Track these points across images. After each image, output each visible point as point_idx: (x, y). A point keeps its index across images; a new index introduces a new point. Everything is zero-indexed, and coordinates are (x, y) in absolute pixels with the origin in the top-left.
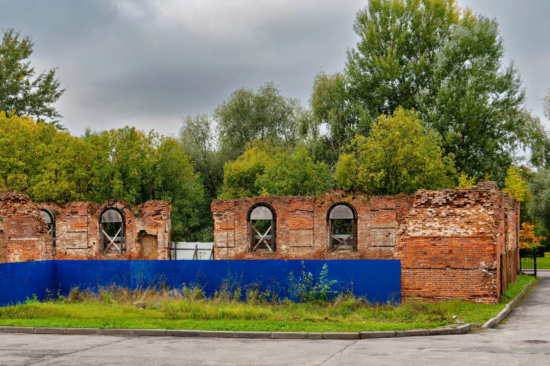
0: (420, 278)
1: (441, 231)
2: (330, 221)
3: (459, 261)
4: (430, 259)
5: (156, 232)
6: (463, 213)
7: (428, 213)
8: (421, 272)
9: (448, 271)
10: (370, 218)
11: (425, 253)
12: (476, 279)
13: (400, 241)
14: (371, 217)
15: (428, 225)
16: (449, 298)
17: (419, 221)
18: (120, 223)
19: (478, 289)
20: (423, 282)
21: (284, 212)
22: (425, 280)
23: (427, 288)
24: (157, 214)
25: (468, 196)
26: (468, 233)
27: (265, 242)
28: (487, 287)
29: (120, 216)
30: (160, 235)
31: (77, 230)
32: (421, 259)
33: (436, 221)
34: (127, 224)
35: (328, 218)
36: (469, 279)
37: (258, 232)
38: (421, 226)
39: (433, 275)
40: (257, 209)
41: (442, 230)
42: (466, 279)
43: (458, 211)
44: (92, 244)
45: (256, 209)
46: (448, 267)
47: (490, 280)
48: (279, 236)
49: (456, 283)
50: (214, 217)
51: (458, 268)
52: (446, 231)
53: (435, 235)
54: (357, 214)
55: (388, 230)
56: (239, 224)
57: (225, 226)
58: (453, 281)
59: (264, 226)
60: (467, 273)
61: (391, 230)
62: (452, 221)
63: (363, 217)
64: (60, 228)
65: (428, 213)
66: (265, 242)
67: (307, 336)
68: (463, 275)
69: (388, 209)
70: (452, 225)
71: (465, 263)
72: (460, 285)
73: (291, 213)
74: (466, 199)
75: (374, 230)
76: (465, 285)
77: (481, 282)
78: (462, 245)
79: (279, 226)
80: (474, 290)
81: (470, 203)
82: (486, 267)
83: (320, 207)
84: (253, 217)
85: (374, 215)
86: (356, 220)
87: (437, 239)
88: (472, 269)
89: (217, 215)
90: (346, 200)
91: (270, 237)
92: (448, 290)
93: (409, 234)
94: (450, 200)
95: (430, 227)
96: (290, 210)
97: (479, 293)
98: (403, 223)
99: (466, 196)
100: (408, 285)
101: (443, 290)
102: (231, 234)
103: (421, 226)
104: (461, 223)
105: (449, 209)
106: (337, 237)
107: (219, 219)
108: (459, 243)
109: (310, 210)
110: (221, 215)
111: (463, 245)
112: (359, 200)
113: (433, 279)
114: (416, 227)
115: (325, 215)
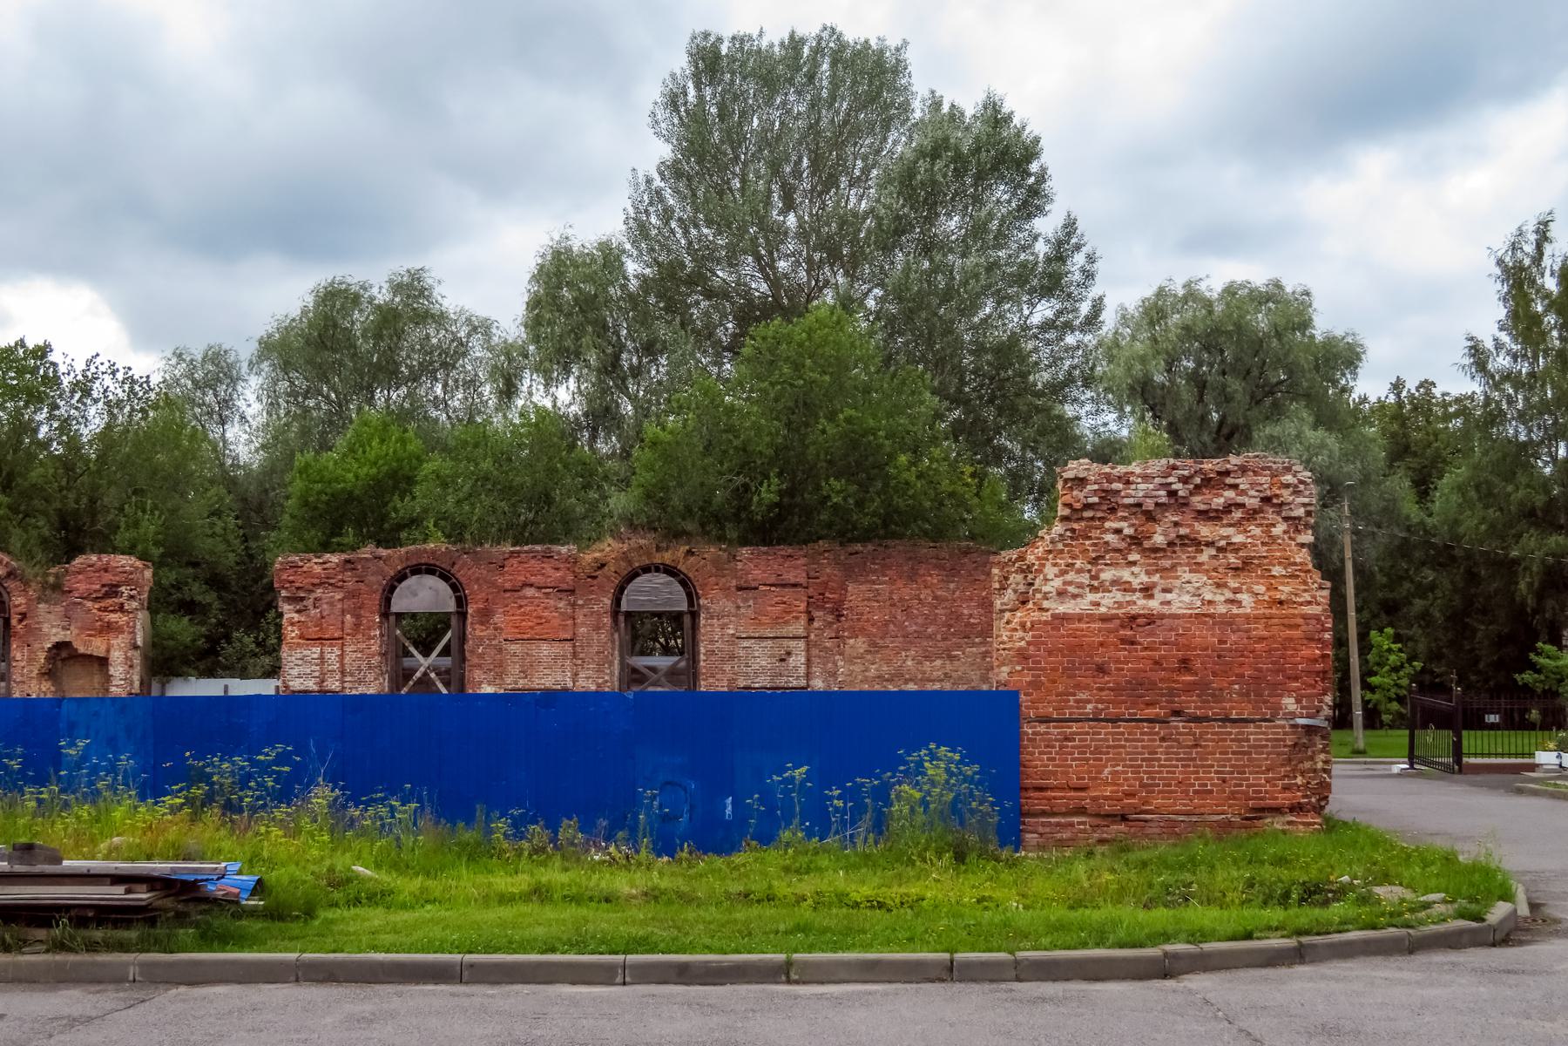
0: (1082, 749)
1: (1151, 597)
2: (621, 618)
4: (1117, 689)
6: (1223, 538)
7: (1109, 537)
8: (1088, 733)
9: (1177, 728)
10: (733, 610)
11: (1101, 669)
12: (1268, 754)
13: (1016, 630)
14: (738, 607)
15: (1107, 575)
16: (1181, 818)
17: (1078, 563)
19: (1275, 785)
20: (1094, 766)
21: (491, 590)
22: (1101, 760)
23: (1107, 784)
24: (107, 596)
25: (1238, 481)
26: (1239, 603)
27: (433, 675)
28: (1299, 780)
30: (117, 656)
32: (1087, 687)
33: (1134, 563)
34: (14, 622)
35: (615, 612)
37: (412, 649)
38: (1085, 579)
39: (1126, 740)
40: (412, 581)
41: (1156, 592)
42: (1233, 753)
43: (1205, 531)
45: (405, 584)
46: (1177, 713)
47: (1312, 758)
48: (472, 660)
49: (1203, 766)
50: (280, 604)
51: (1206, 719)
52: (1169, 596)
53: (1134, 610)
54: (698, 598)
55: (786, 642)
56: (357, 626)
57: (313, 631)
58: (1194, 759)
59: (427, 632)
60: (1238, 733)
61: (793, 643)
62: (1188, 564)
63: (715, 608)
65: (1109, 537)
66: (433, 675)
67: (951, 969)
68: (1225, 740)
69: (784, 586)
70: (1187, 576)
72: (1217, 772)
73: (508, 595)
74: (1230, 494)
75: (746, 644)
76: (1232, 773)
77: (1282, 765)
78: (1220, 642)
79: (475, 631)
80: (1260, 792)
81: (1242, 505)
83: (594, 578)
84: (400, 604)
85: (745, 600)
86: (694, 615)
88: (1253, 721)
89: (289, 600)
90: (666, 557)
91: (447, 662)
92: (1176, 792)
93: (1046, 604)
94: (1181, 493)
95: (1115, 582)
96: (508, 585)
97: (1277, 798)
98: (1016, 572)
99: (1229, 481)
100: (1046, 775)
101: (1160, 792)
102: (332, 654)
103: (1085, 579)
104: (1215, 570)
105: (1176, 524)
106: (641, 662)
107: (298, 612)
108: (1213, 635)
109: (564, 586)
110: (302, 599)
111: (1225, 642)
112: (702, 558)
113: (1128, 753)
114: (1070, 583)
115: (607, 601)
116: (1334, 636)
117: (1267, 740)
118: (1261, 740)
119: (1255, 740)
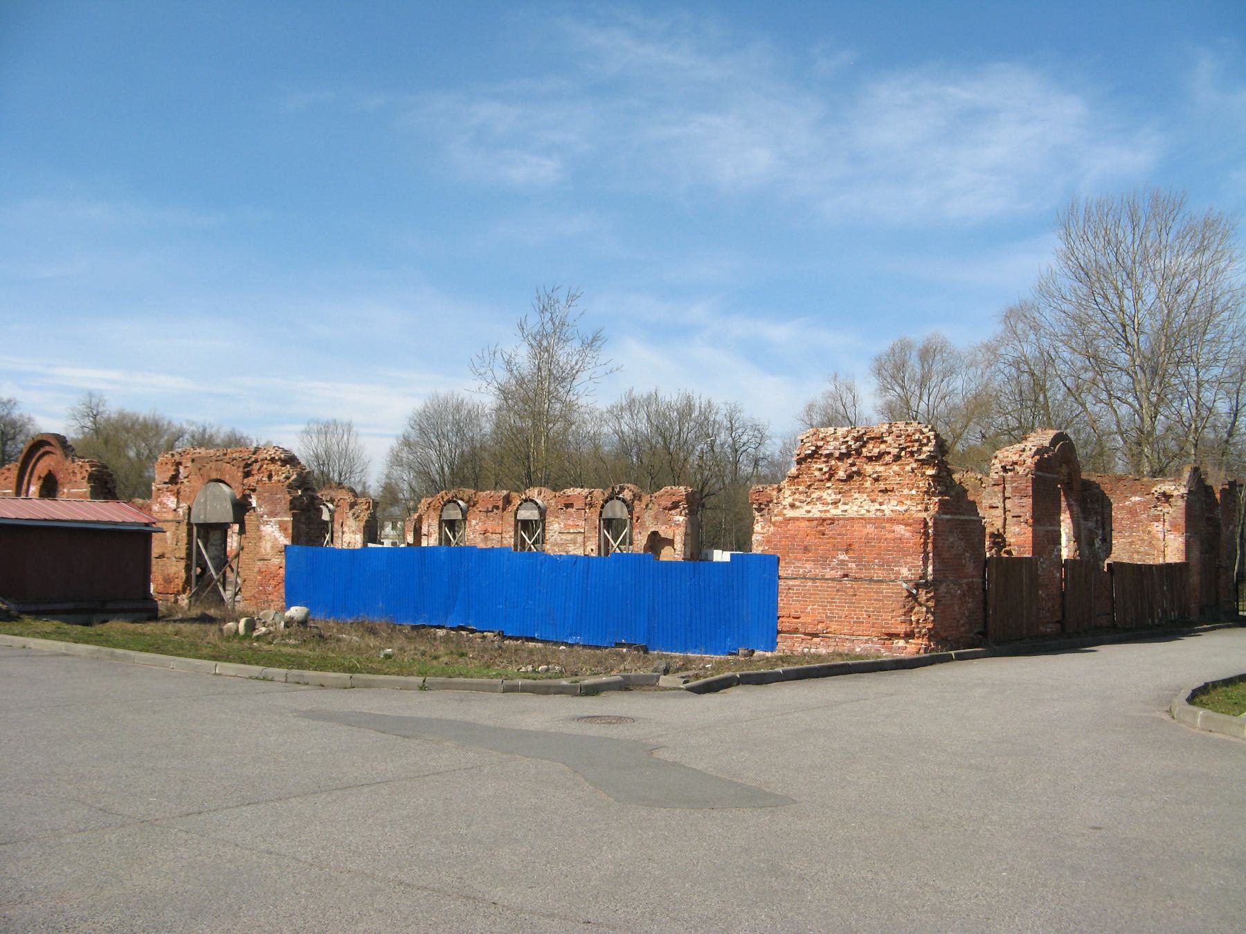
5: (672, 535)
7: (817, 473)
9: (846, 584)
18: (625, 520)
22: (807, 601)
29: (625, 510)
31: (571, 531)
36: (880, 600)
42: (875, 600)
44: (590, 551)
49: (858, 607)
64: (551, 528)
68: (870, 592)
70: (856, 495)
71: (874, 569)
82: (910, 578)
101: (836, 621)
103: (802, 497)
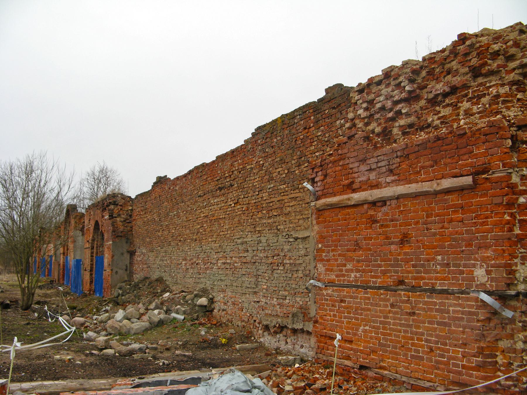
3: (423, 266)
12: (464, 327)
42: (438, 323)
47: (511, 336)
58: (410, 326)
68: (431, 310)
87: (378, 204)
88: (453, 293)
116: (320, 243)
117: (463, 313)
118: (458, 312)
119: (454, 312)
